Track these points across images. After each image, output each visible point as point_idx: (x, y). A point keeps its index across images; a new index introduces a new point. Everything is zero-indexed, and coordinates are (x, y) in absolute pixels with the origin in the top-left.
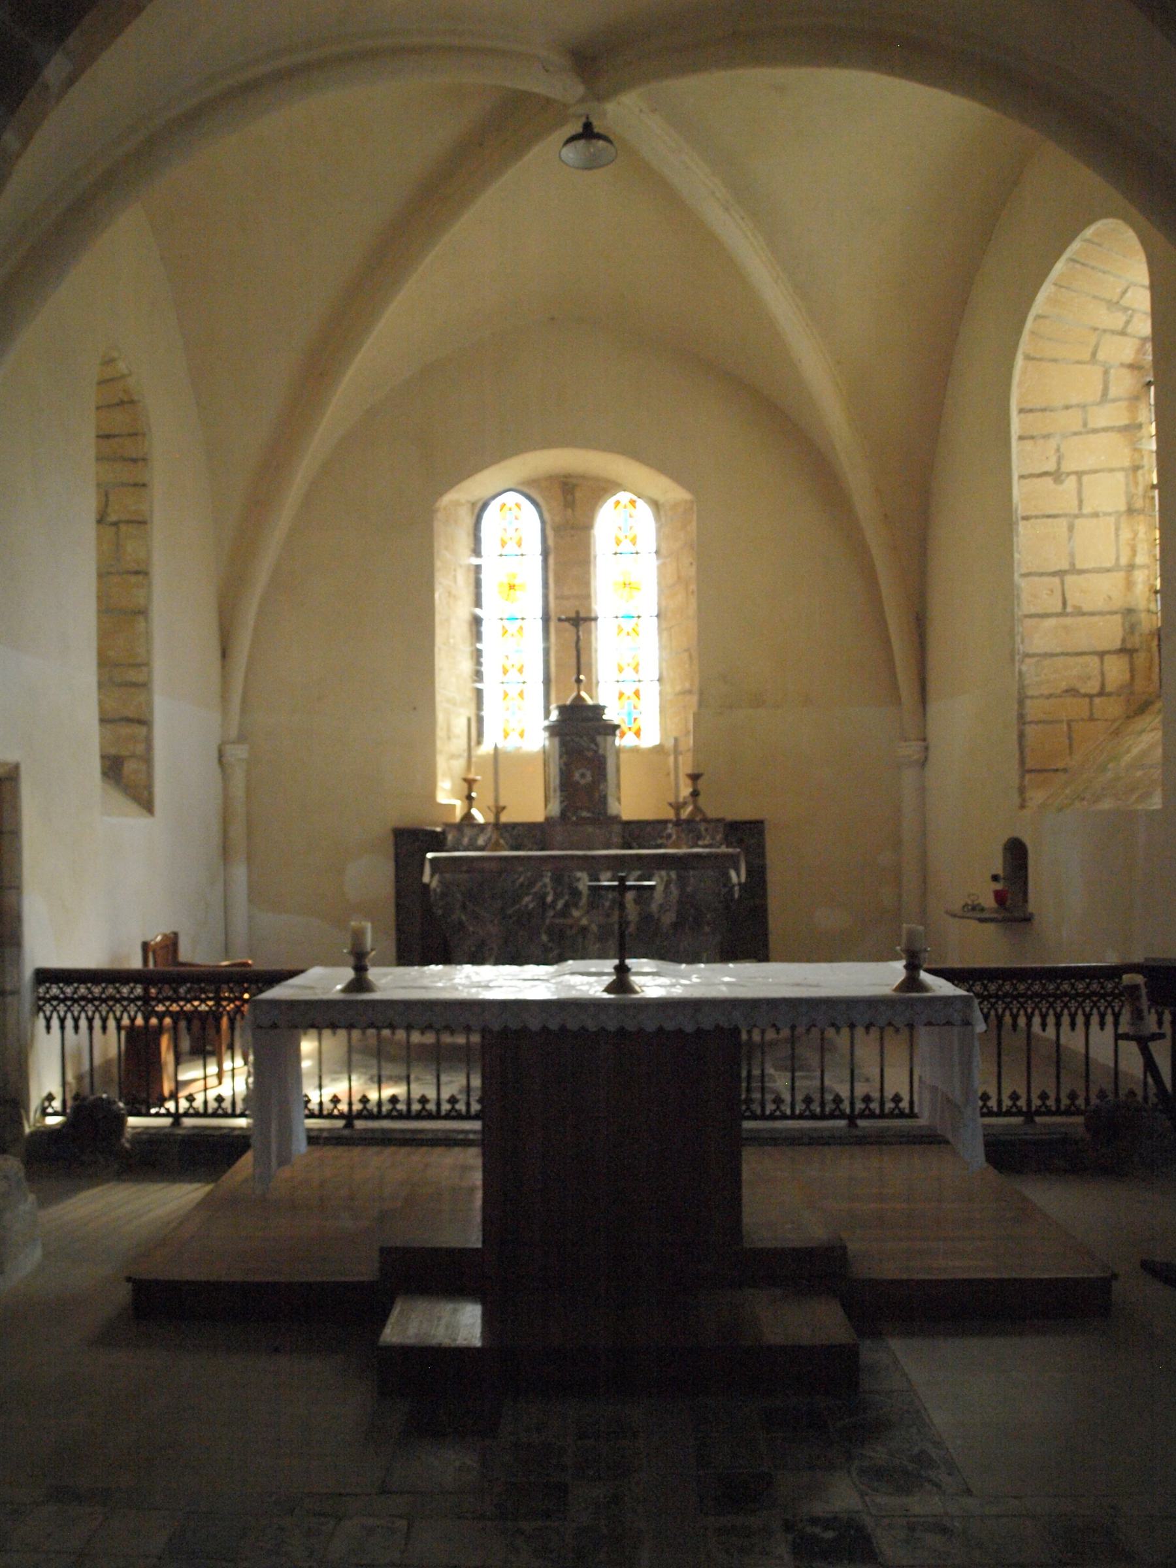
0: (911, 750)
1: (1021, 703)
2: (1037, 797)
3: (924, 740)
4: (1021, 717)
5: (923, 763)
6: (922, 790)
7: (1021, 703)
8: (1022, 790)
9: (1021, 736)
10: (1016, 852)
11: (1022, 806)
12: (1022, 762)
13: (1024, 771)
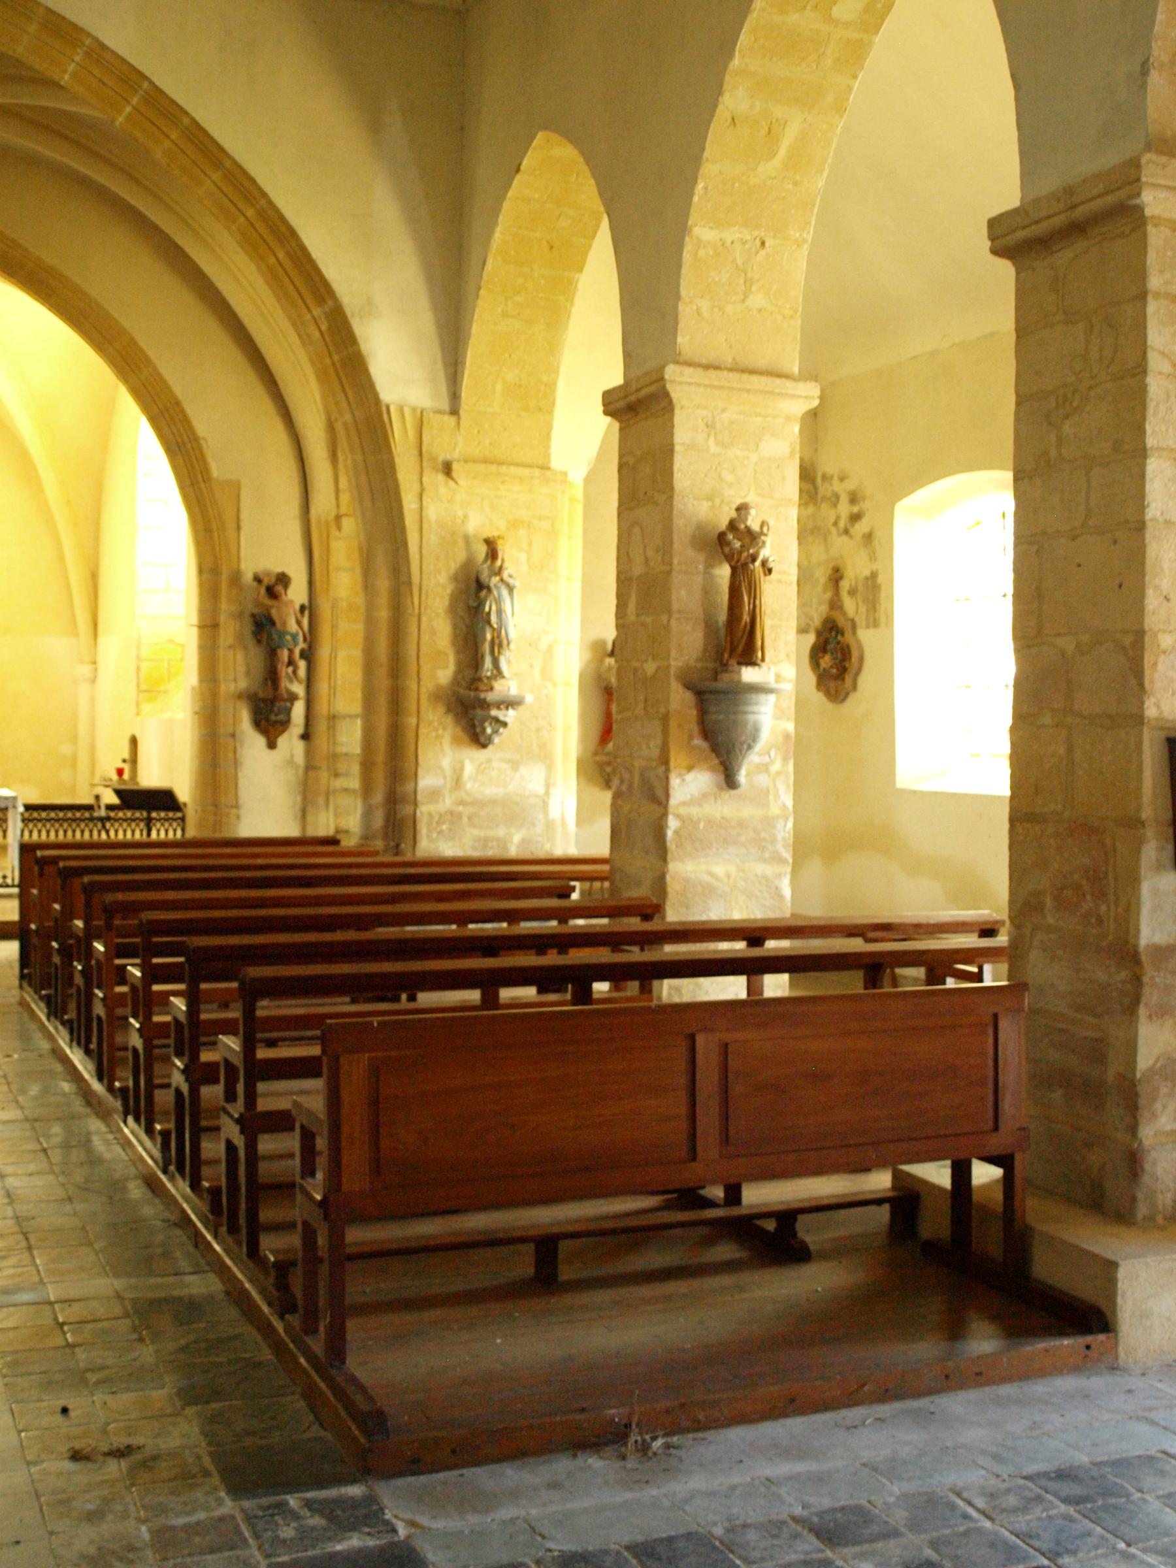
0: (85, 670)
1: (139, 647)
2: (146, 708)
3: (95, 663)
4: (138, 658)
5: (93, 680)
6: (93, 699)
7: (139, 647)
8: (138, 704)
9: (138, 668)
10: (134, 741)
11: (138, 714)
12: (138, 686)
13: (140, 691)
